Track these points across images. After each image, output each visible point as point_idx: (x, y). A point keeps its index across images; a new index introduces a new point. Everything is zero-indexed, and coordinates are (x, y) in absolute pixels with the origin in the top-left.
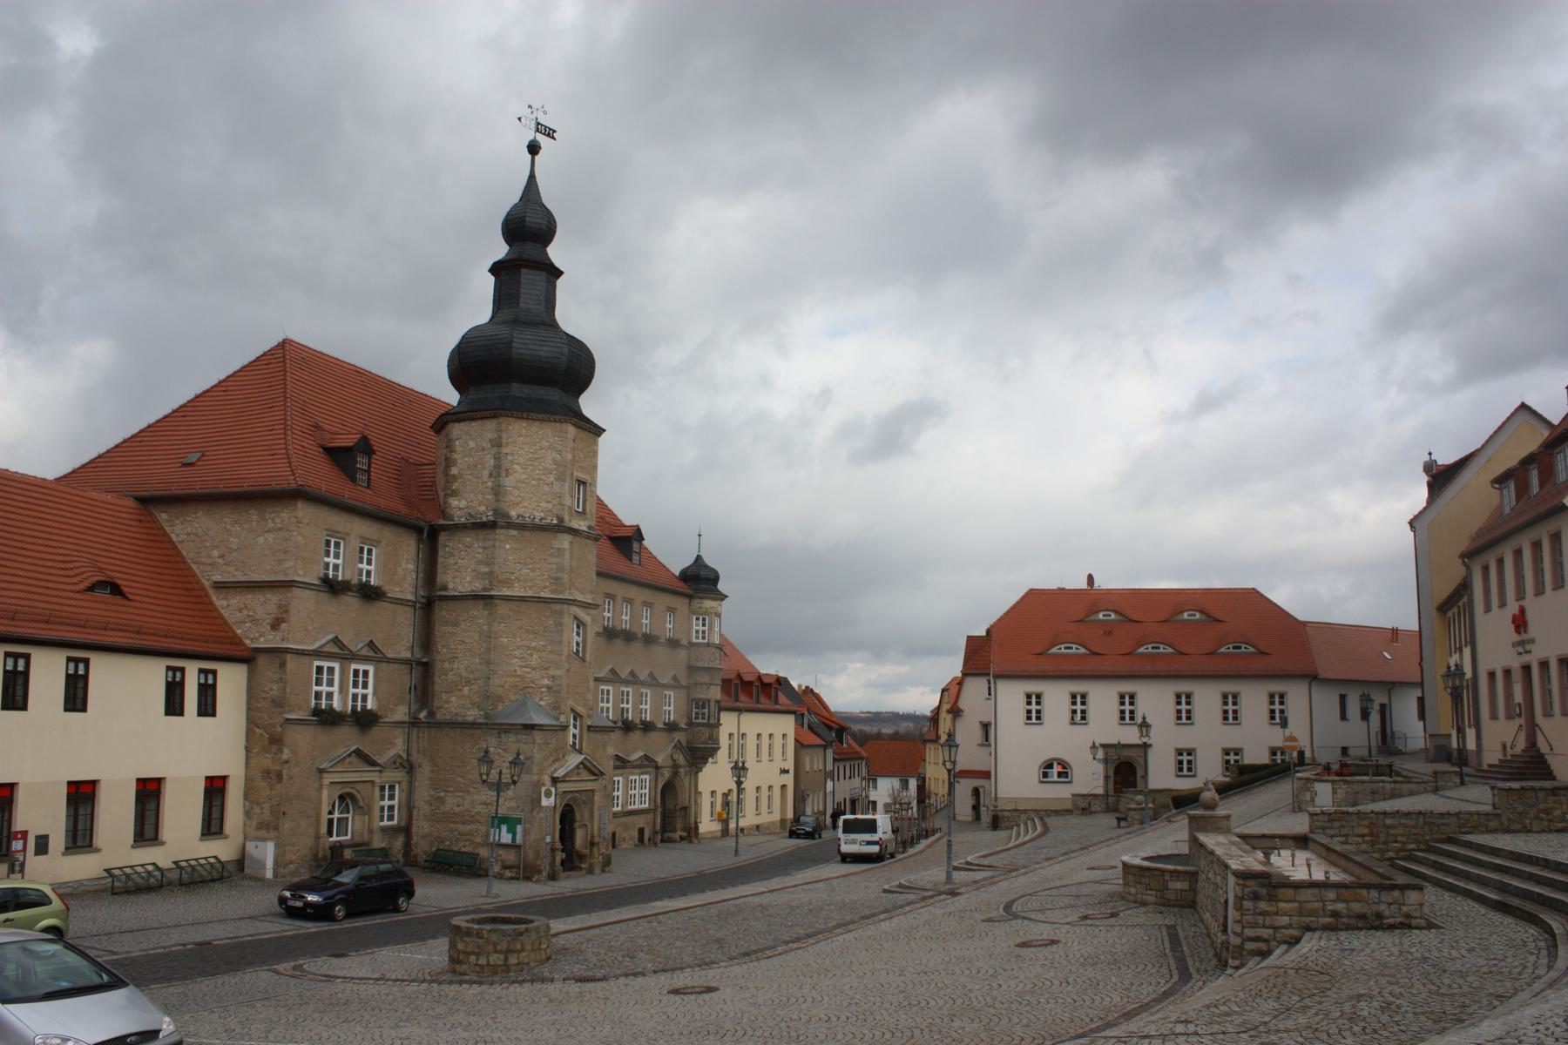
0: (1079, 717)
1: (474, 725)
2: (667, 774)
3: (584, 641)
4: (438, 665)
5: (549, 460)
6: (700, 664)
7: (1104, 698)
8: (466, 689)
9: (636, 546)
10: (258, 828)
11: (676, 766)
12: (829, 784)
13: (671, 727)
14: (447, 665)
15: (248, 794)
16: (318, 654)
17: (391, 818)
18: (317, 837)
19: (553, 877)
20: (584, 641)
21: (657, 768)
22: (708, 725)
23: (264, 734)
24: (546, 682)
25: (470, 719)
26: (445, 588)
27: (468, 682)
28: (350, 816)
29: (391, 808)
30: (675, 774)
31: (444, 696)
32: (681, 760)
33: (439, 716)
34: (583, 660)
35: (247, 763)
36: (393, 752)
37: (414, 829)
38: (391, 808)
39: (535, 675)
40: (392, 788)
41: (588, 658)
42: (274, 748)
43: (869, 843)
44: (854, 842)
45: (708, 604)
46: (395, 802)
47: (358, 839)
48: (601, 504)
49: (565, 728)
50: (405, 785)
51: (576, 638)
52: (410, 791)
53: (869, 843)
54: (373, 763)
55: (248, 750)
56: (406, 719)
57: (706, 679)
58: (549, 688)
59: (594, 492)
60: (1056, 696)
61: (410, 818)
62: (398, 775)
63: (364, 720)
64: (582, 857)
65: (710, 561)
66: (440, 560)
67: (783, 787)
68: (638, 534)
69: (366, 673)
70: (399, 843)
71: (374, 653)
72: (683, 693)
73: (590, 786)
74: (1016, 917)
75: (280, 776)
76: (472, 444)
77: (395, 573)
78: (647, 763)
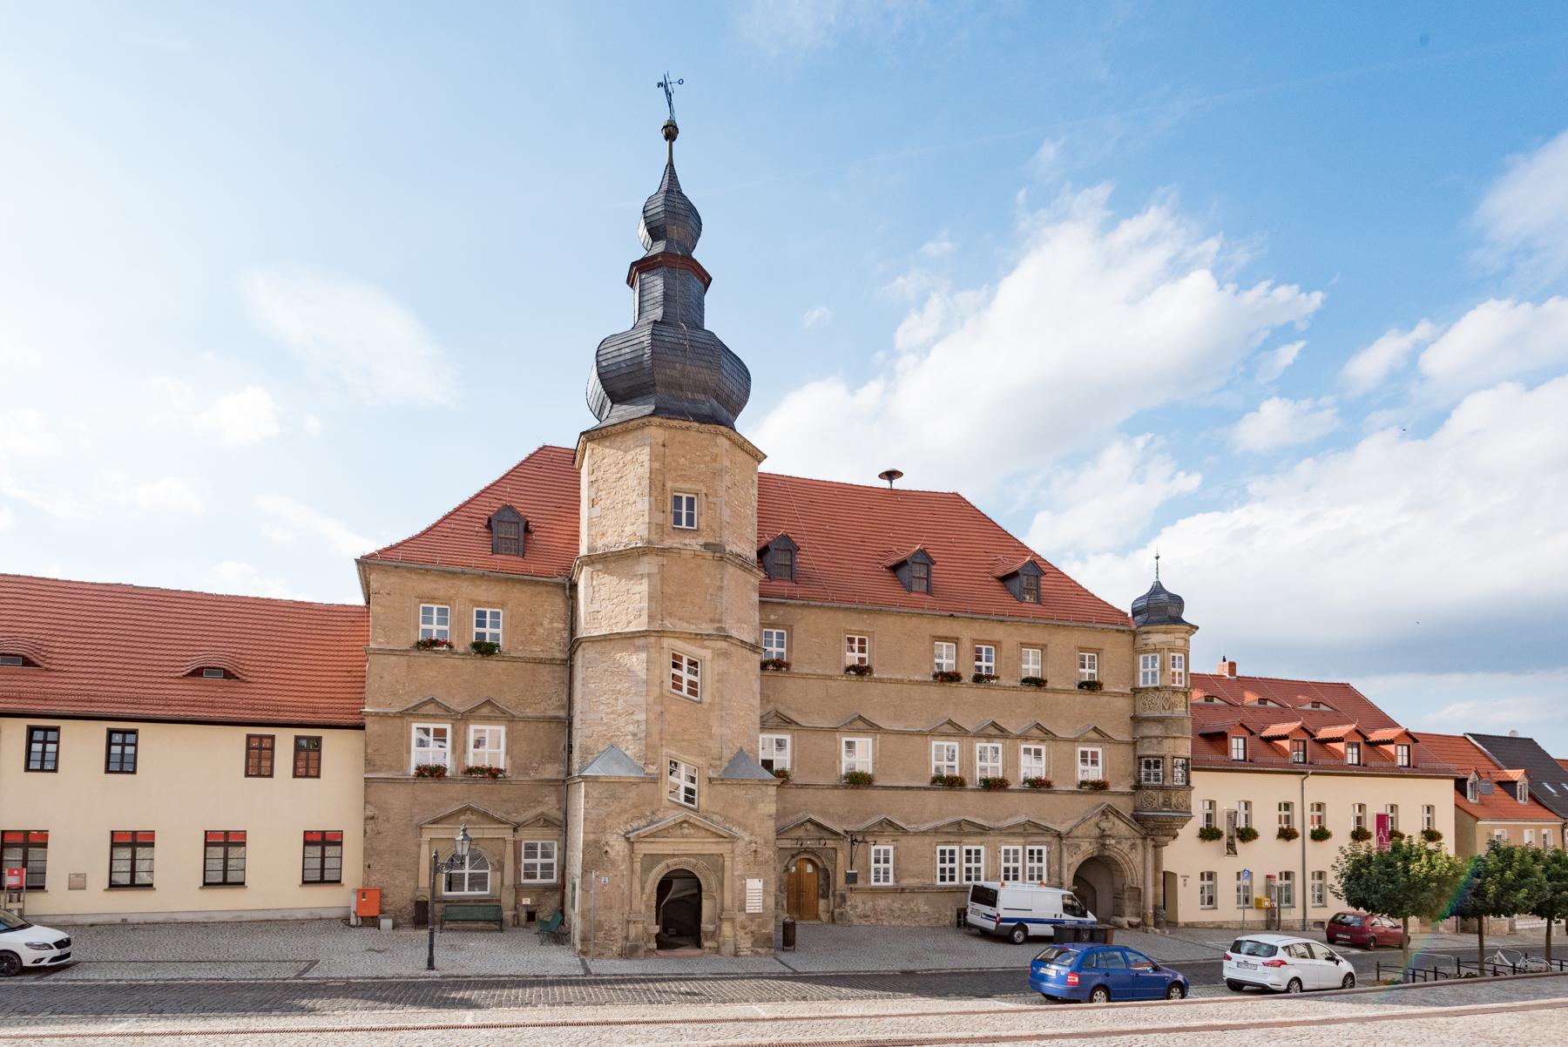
6: (1145, 714)
19: (629, 953)
36: (539, 810)
57: (1156, 730)
58: (634, 735)
65: (1170, 587)
77: (533, 633)
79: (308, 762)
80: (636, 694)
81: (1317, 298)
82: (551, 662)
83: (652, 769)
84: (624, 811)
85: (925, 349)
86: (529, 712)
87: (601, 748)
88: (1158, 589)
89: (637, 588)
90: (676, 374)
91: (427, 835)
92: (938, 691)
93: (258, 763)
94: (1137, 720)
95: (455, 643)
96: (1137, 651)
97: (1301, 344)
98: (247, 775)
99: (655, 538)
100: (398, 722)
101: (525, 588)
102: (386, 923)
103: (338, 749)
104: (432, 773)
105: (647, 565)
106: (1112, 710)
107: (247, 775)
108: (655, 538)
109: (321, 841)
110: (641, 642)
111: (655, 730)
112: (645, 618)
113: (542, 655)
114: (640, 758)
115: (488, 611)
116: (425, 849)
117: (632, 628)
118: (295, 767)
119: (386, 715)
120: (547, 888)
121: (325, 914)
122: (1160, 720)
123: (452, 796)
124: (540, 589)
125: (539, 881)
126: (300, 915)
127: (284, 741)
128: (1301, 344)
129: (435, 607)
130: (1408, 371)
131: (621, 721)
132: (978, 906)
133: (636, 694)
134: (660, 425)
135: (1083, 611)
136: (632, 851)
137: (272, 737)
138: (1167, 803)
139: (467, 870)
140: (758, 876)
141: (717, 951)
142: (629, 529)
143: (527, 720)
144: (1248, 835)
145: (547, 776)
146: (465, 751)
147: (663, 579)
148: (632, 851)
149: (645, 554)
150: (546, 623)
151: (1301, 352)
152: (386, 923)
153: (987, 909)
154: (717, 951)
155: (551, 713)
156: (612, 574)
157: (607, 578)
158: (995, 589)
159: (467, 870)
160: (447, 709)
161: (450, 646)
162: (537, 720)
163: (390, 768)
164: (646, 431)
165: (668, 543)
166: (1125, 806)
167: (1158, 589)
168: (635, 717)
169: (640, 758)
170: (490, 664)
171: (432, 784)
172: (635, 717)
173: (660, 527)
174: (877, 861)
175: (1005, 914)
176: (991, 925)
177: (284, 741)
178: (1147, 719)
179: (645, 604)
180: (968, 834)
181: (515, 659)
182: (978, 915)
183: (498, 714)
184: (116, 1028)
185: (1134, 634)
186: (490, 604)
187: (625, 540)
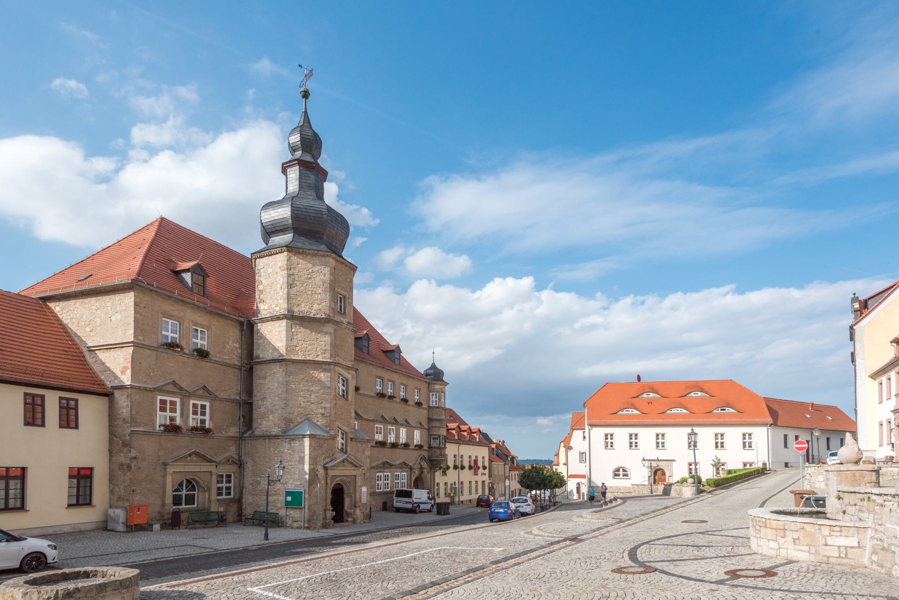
0: (633, 443)
1: (276, 437)
2: (417, 473)
3: (347, 389)
4: (255, 404)
5: (318, 279)
6: (434, 417)
7: (647, 435)
8: (271, 416)
9: (397, 355)
10: (118, 501)
11: (421, 468)
12: (507, 482)
13: (420, 447)
14: (260, 403)
15: (112, 478)
16: (160, 390)
17: (229, 494)
18: (163, 505)
19: (325, 526)
20: (347, 389)
21: (411, 469)
22: (439, 448)
23: (117, 440)
24: (321, 411)
25: (273, 433)
26: (258, 357)
27: (272, 412)
28: (196, 493)
29: (229, 488)
30: (422, 472)
31: (259, 421)
32: (425, 465)
33: (256, 433)
34: (347, 399)
35: (110, 460)
36: (227, 454)
37: (244, 500)
38: (229, 488)
39: (314, 407)
40: (229, 476)
41: (350, 398)
42: (125, 449)
43: (407, 503)
44: (400, 502)
45: (437, 387)
46: (232, 485)
47: (201, 506)
48: (356, 312)
49: (333, 438)
50: (237, 475)
51: (341, 387)
52: (241, 477)
53: (407, 503)
54: (210, 461)
55: (110, 451)
56: (238, 435)
57: (438, 424)
58: (323, 414)
59: (352, 303)
60: (621, 435)
61: (241, 493)
62: (230, 469)
63: (202, 431)
64: (348, 515)
65: (438, 366)
66: (255, 341)
67: (483, 482)
68: (397, 349)
69: (203, 407)
70: (234, 509)
71: (206, 392)
72: (426, 432)
73: (353, 473)
74: (648, 569)
75: (129, 467)
76: (270, 270)
77: (224, 347)
78: (404, 465)
79: (69, 418)
80: (323, 393)
81: (377, 221)
82: (232, 366)
83: (332, 432)
84: (323, 454)
85: (152, 150)
86: (222, 395)
87: (300, 420)
88: (433, 367)
89: (323, 339)
90: (334, 232)
91: (170, 470)
92: (377, 401)
93: (34, 416)
94: (430, 420)
95: (184, 345)
96: (430, 391)
97: (365, 239)
98: (60, 427)
99: (331, 315)
100: (150, 394)
101: (221, 320)
102: (157, 527)
103: (90, 409)
104: (172, 429)
105: (330, 328)
106: (423, 413)
107: (60, 427)
108: (331, 315)
109: (82, 477)
110: (327, 367)
111: (333, 412)
112: (328, 355)
113: (229, 362)
114: (326, 426)
115: (199, 329)
116: (169, 479)
117: (320, 359)
118: (60, 424)
119: (145, 389)
120: (231, 501)
121: (83, 528)
122: (439, 420)
123: (184, 444)
124: (228, 322)
125: (224, 497)
126: (66, 530)
127: (52, 400)
128: (365, 239)
129: (170, 321)
130: (401, 262)
131: (314, 407)
132: (400, 499)
133: (323, 393)
134: (334, 259)
135: (408, 370)
136: (327, 474)
137: (76, 401)
138: (441, 454)
139: (184, 492)
140: (364, 485)
141: (354, 522)
142: (316, 307)
143: (221, 400)
144: (463, 468)
145: (231, 434)
146: (188, 417)
147: (335, 337)
148: (327, 474)
149: (329, 322)
150: (230, 342)
151: (363, 243)
152: (157, 527)
153: (406, 500)
154: (354, 522)
155: (233, 397)
156: (306, 328)
157: (302, 329)
158: (382, 354)
159: (184, 492)
160: (181, 389)
161: (182, 349)
162: (227, 400)
163: (146, 425)
164: (327, 259)
165: (336, 318)
166: (426, 454)
167: (433, 367)
168: (323, 405)
169: (326, 426)
170: (204, 364)
171: (171, 437)
172: (323, 405)
173: (333, 309)
174: (229, 488)
175: (415, 501)
176: (410, 506)
177: (52, 400)
178: (434, 420)
179: (328, 348)
180: (386, 468)
181: (216, 362)
182: (399, 503)
183: (207, 394)
184: (303, 559)
185: (429, 384)
186: (202, 326)
187: (314, 312)
